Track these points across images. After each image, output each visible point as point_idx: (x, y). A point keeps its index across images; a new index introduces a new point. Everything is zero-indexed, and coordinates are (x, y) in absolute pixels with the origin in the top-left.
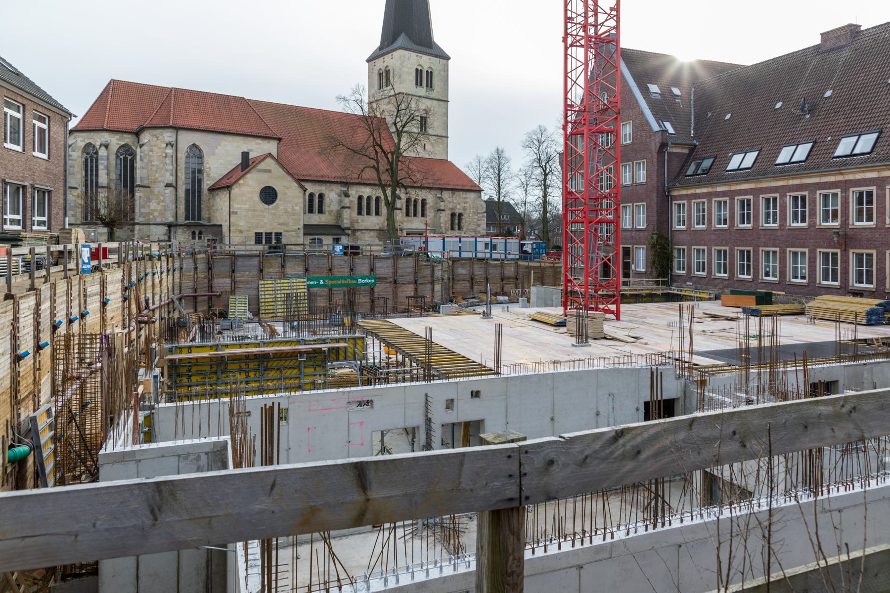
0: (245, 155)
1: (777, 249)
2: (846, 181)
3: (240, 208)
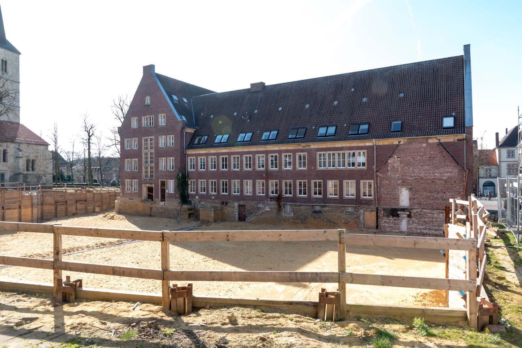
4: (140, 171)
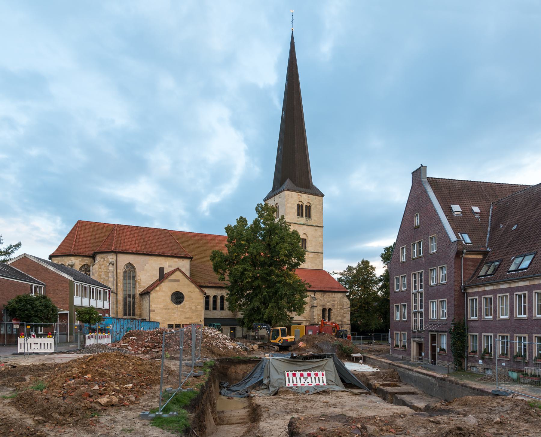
0: (162, 270)
3: (157, 307)
4: (409, 321)
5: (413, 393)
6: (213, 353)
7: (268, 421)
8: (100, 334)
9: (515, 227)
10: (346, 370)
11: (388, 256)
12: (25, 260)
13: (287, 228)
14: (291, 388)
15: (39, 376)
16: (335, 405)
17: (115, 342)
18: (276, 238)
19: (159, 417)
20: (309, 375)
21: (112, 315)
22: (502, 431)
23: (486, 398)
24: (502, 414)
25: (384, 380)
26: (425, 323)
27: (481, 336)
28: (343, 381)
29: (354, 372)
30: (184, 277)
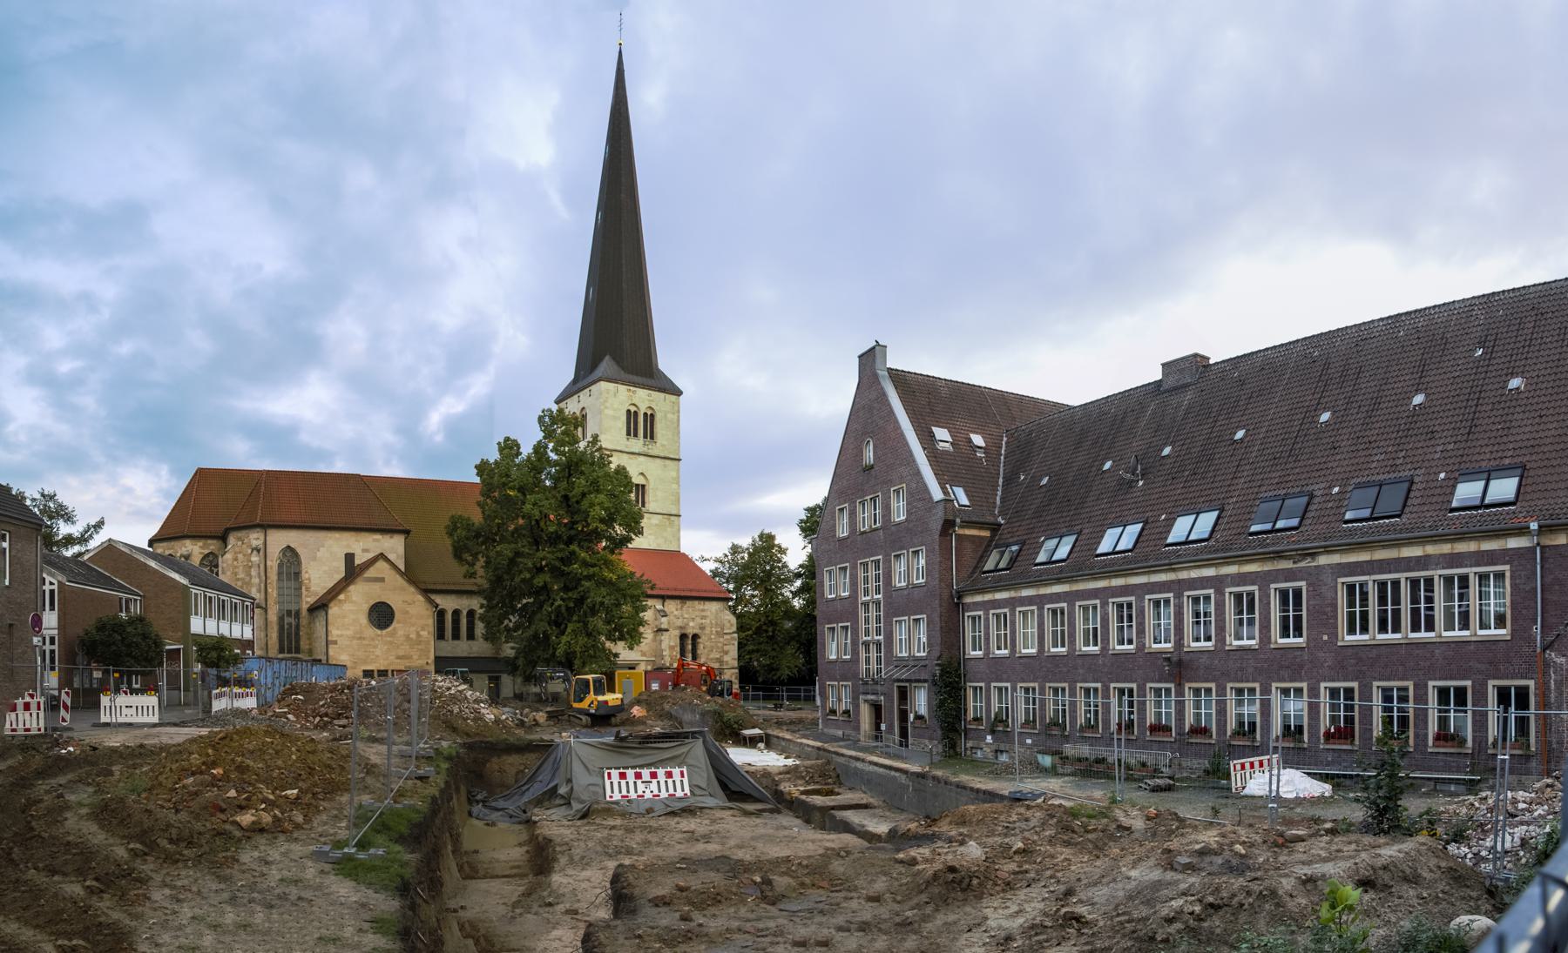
0: (350, 558)
1: (1099, 685)
2: (1179, 581)
4: (855, 659)
5: (866, 807)
6: (454, 730)
7: (570, 872)
8: (236, 690)
9: (1045, 481)
10: (731, 764)
11: (812, 524)
12: (110, 550)
13: (603, 462)
14: (616, 803)
15: (135, 767)
16: (707, 838)
17: (263, 706)
18: (581, 483)
19: (349, 858)
20: (654, 775)
21: (258, 652)
22: (1026, 867)
23: (998, 806)
24: (1027, 834)
25: (808, 783)
26: (887, 665)
27: (988, 689)
28: (724, 786)
29: (751, 769)
30: (393, 572)
